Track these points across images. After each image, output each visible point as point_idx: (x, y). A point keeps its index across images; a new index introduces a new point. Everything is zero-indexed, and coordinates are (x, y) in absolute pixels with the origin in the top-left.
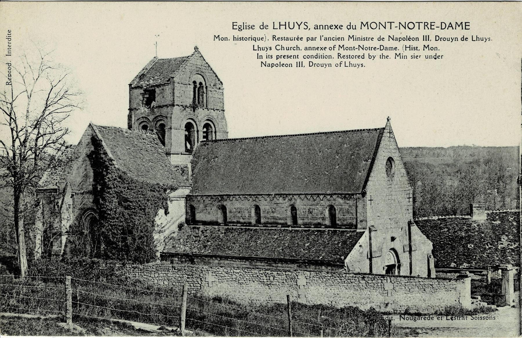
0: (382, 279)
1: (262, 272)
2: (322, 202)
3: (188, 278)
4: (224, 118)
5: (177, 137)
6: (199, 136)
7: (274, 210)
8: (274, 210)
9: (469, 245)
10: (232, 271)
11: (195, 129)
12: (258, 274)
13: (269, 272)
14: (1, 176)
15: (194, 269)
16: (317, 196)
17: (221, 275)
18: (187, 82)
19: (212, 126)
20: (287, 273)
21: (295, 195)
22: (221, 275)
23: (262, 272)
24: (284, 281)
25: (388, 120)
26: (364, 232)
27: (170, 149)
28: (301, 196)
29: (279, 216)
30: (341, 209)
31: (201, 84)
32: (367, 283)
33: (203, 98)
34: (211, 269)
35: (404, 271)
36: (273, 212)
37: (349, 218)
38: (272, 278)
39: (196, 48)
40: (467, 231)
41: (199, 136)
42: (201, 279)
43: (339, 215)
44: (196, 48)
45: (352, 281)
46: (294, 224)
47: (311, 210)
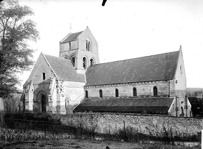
0: (199, 120)
1: (132, 117)
2: (150, 85)
3: (89, 120)
4: (98, 57)
5: (79, 62)
6: (88, 64)
7: (125, 90)
8: (125, 90)
9: (198, 108)
10: (115, 116)
11: (87, 60)
12: (130, 118)
13: (136, 117)
14: (107, 147)
15: (93, 116)
16: (147, 82)
17: (109, 119)
18: (84, 40)
19: (94, 60)
20: (146, 117)
21: (136, 82)
22: (109, 119)
23: (132, 117)
24: (145, 122)
25: (181, 47)
26: (174, 98)
27: (77, 67)
28: (139, 83)
29: (127, 93)
30: (160, 88)
31: (89, 42)
32: (191, 123)
33: (90, 48)
34: (102, 115)
35: (185, 116)
36: (124, 91)
37: (166, 92)
38: (137, 120)
39: (87, 27)
40: (196, 102)
41: (88, 64)
42: (97, 121)
43: (159, 91)
44: (87, 27)
45: (182, 121)
46: (134, 96)
47: (144, 89)
